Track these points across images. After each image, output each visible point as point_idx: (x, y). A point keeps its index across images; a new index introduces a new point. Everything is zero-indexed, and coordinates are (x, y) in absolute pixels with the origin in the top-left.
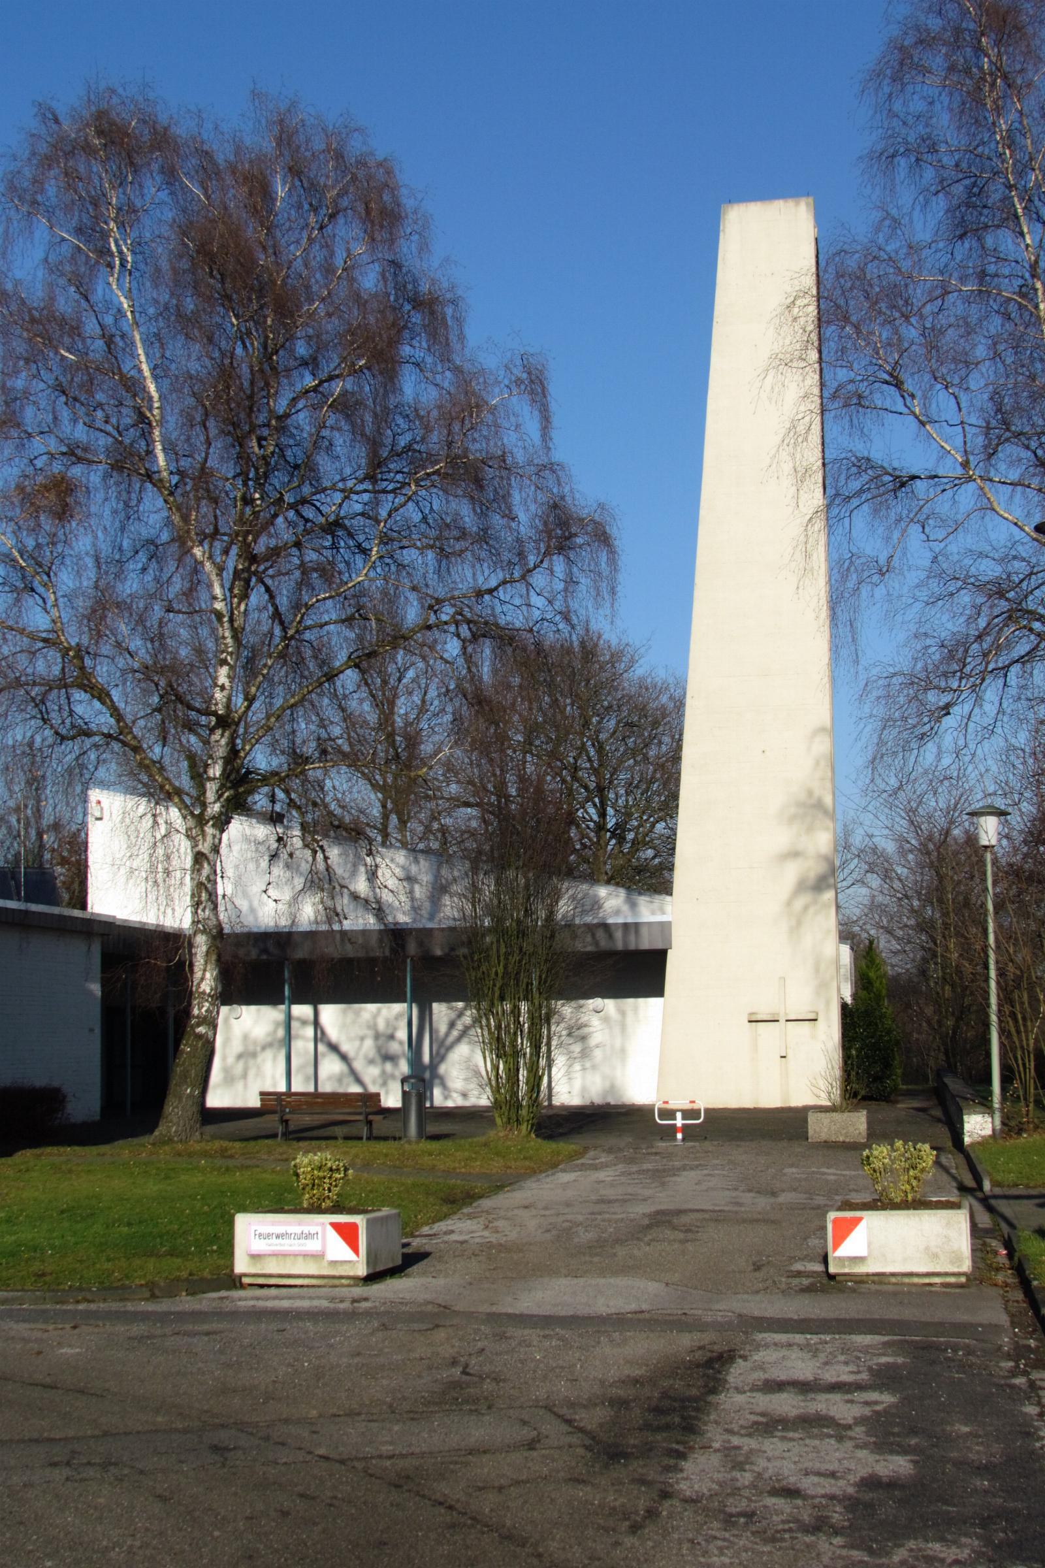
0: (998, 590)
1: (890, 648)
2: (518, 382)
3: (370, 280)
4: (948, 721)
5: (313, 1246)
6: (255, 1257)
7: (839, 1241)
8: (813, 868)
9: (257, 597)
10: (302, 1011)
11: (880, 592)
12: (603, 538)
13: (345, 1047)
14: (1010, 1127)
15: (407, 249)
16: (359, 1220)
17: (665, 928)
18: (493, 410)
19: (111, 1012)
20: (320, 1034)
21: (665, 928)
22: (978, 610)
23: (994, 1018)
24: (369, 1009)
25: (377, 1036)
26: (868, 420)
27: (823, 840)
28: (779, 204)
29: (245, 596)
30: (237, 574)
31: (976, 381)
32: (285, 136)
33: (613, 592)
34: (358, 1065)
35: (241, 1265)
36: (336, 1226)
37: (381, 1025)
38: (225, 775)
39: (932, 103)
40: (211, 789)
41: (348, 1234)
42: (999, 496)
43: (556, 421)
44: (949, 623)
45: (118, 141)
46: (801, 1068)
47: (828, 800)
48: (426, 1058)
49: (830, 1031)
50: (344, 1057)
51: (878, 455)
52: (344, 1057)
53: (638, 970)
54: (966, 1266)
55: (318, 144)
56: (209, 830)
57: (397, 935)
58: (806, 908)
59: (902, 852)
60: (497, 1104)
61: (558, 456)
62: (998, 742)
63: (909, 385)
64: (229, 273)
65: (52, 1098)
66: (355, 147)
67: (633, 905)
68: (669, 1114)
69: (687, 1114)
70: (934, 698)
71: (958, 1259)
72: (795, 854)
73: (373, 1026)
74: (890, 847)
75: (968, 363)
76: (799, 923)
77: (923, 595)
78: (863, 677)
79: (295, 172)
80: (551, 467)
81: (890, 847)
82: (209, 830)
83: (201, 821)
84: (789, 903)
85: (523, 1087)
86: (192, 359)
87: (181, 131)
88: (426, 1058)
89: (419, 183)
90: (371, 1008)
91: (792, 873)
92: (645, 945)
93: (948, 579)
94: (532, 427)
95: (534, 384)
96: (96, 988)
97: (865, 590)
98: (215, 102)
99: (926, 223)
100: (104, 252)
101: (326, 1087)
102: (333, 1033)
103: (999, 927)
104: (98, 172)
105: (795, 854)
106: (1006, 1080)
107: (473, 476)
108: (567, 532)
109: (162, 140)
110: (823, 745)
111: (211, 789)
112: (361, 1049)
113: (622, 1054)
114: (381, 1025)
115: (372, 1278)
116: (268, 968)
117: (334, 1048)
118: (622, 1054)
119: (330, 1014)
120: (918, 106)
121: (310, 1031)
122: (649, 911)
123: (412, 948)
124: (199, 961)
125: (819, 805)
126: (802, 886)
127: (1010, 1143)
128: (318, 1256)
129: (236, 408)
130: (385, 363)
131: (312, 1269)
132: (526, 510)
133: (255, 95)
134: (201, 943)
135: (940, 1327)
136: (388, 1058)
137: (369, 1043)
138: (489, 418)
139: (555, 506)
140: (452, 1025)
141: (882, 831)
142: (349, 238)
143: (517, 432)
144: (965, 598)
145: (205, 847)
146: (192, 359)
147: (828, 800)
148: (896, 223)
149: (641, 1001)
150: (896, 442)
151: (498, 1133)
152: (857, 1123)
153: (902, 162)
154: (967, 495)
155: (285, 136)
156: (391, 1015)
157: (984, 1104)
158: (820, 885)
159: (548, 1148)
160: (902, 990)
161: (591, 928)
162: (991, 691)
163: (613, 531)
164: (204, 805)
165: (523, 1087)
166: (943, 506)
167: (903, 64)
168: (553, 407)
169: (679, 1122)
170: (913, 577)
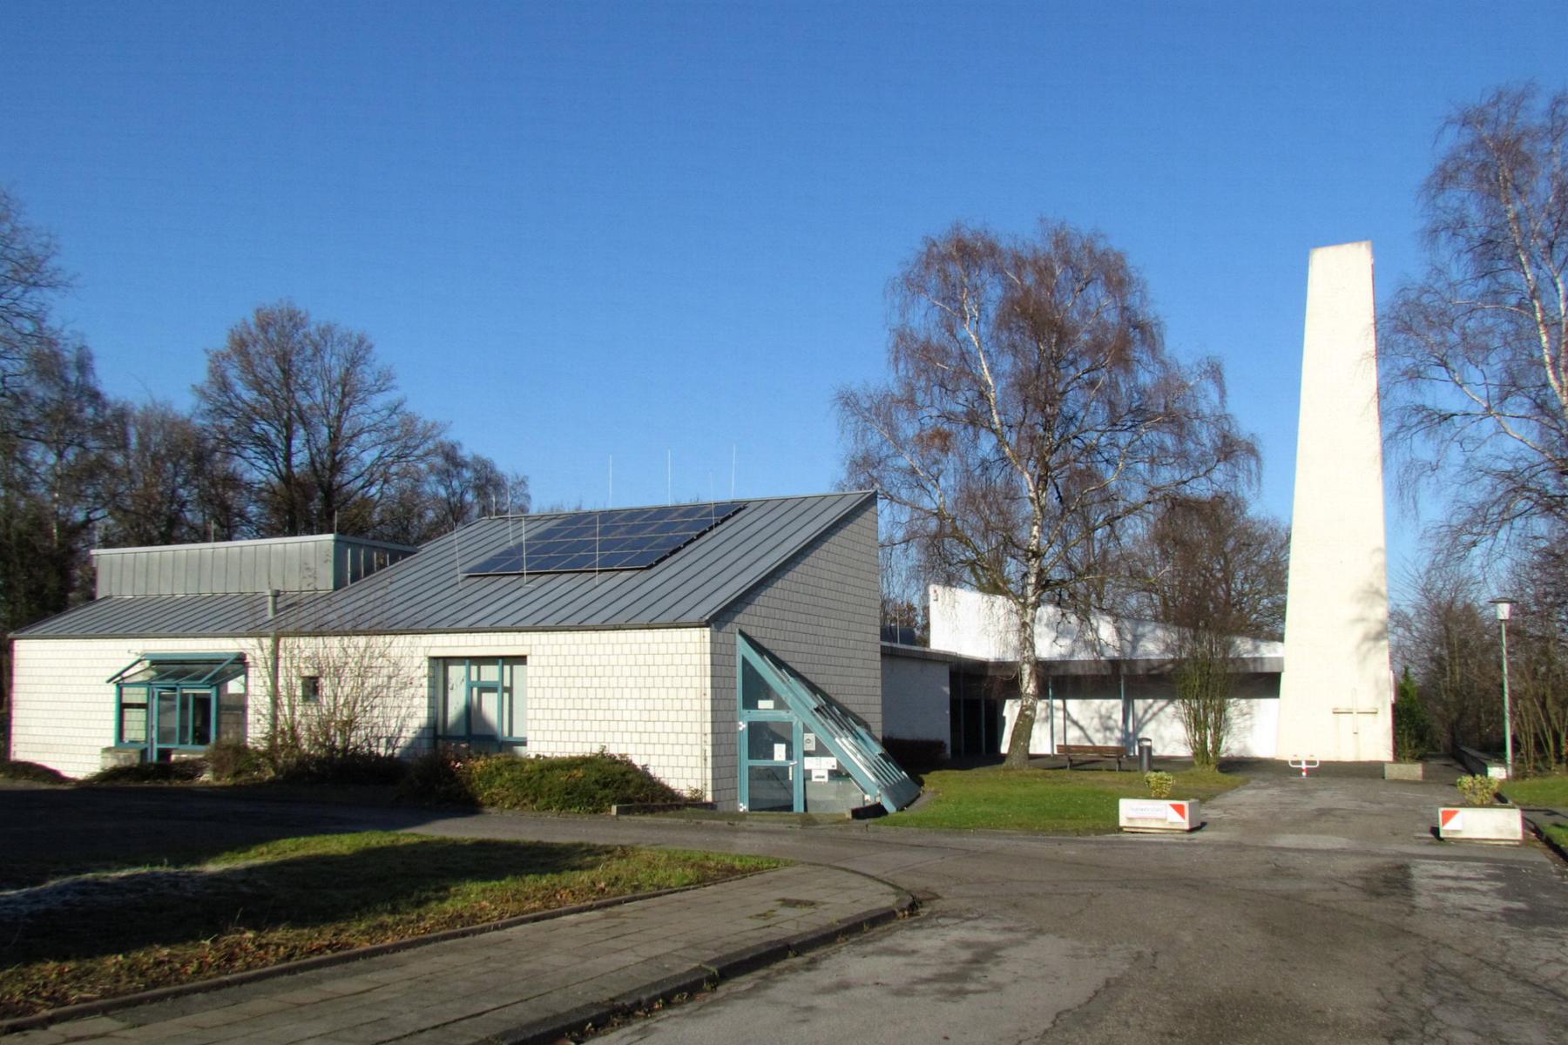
0: (1507, 476)
1: (1435, 509)
2: (1206, 372)
3: (1112, 317)
4: (1475, 551)
5: (1160, 815)
6: (1130, 819)
7: (1446, 820)
8: (1375, 627)
9: (1051, 488)
10: (1058, 703)
11: (1433, 480)
12: (1251, 451)
13: (1082, 723)
14: (1519, 774)
15: (1134, 301)
16: (1185, 803)
17: (1280, 661)
18: (1191, 388)
19: (954, 704)
20: (1067, 716)
21: (1280, 661)
22: (1495, 488)
23: (1507, 715)
24: (1096, 702)
25: (1101, 717)
26: (1424, 385)
27: (1380, 612)
28: (1348, 246)
29: (1044, 489)
30: (1040, 477)
31: (1493, 359)
32: (1060, 242)
33: (1259, 479)
34: (1090, 733)
35: (1123, 822)
36: (1174, 806)
37: (1103, 711)
38: (1038, 582)
39: (1464, 200)
40: (1030, 590)
41: (1179, 809)
42: (1511, 425)
43: (1230, 391)
44: (1475, 495)
45: (969, 253)
46: (1372, 740)
47: (1383, 589)
48: (1131, 729)
49: (1385, 720)
50: (1081, 728)
51: (1429, 403)
52: (1081, 728)
53: (1267, 683)
54: (1519, 836)
55: (1077, 245)
56: (1030, 611)
57: (1114, 663)
58: (1369, 650)
59: (1419, 615)
60: (1195, 754)
61: (1228, 411)
62: (1507, 561)
63: (1452, 365)
64: (1034, 319)
65: (938, 746)
66: (1101, 246)
67: (1256, 648)
68: (1299, 763)
69: (1308, 763)
70: (1467, 538)
71: (1515, 833)
72: (1362, 620)
73: (1099, 712)
74: (1411, 612)
75: (1487, 349)
76: (1365, 658)
77: (1459, 480)
78: (1421, 529)
79: (1066, 262)
80: (1226, 417)
81: (1411, 612)
82: (1030, 611)
83: (1024, 606)
84: (1358, 647)
85: (1210, 746)
86: (1007, 364)
87: (1004, 244)
88: (1131, 729)
89: (1139, 260)
90: (1097, 702)
91: (1359, 631)
92: (1267, 669)
93: (1473, 472)
94: (1214, 397)
95: (1215, 373)
96: (947, 690)
97: (1423, 480)
98: (1017, 227)
99: (1459, 269)
100: (962, 311)
101: (1070, 742)
102: (1075, 716)
103: (1511, 664)
104: (955, 270)
105: (1362, 620)
106: (1516, 749)
107: (1177, 422)
108: (1230, 449)
109: (992, 250)
110: (1379, 559)
111: (1030, 590)
112: (1092, 725)
113: (1257, 729)
114: (1103, 711)
115: (1191, 830)
116: (1060, 681)
117: (1075, 723)
118: (1257, 729)
119: (1073, 705)
120: (1455, 203)
121: (1061, 714)
122: (1268, 651)
123: (1124, 670)
124: (1026, 678)
125: (1377, 592)
126: (1366, 638)
127: (1518, 783)
128: (1163, 820)
129: (1038, 392)
130: (1122, 360)
131: (1160, 825)
132: (1206, 437)
133: (1042, 220)
134: (1027, 669)
135: (1513, 861)
136: (1108, 729)
137: (1096, 721)
138: (1189, 393)
139: (1225, 437)
140: (1146, 712)
141: (1409, 600)
142: (1097, 294)
143: (1208, 401)
144: (1487, 480)
145: (1028, 620)
146: (1007, 364)
147: (1383, 589)
148: (1440, 272)
149: (1263, 701)
150: (1441, 395)
151: (1197, 770)
152: (1415, 770)
153: (1443, 236)
154: (1488, 425)
155: (1060, 242)
156: (1114, 706)
157: (1501, 761)
158: (1378, 637)
159: (1227, 778)
160: (1423, 695)
161: (1255, 660)
162: (1502, 534)
163: (1259, 448)
164: (1026, 598)
165: (1210, 746)
166: (1471, 430)
167: (1445, 178)
168: (1227, 384)
169: (1304, 766)
170: (1452, 470)
